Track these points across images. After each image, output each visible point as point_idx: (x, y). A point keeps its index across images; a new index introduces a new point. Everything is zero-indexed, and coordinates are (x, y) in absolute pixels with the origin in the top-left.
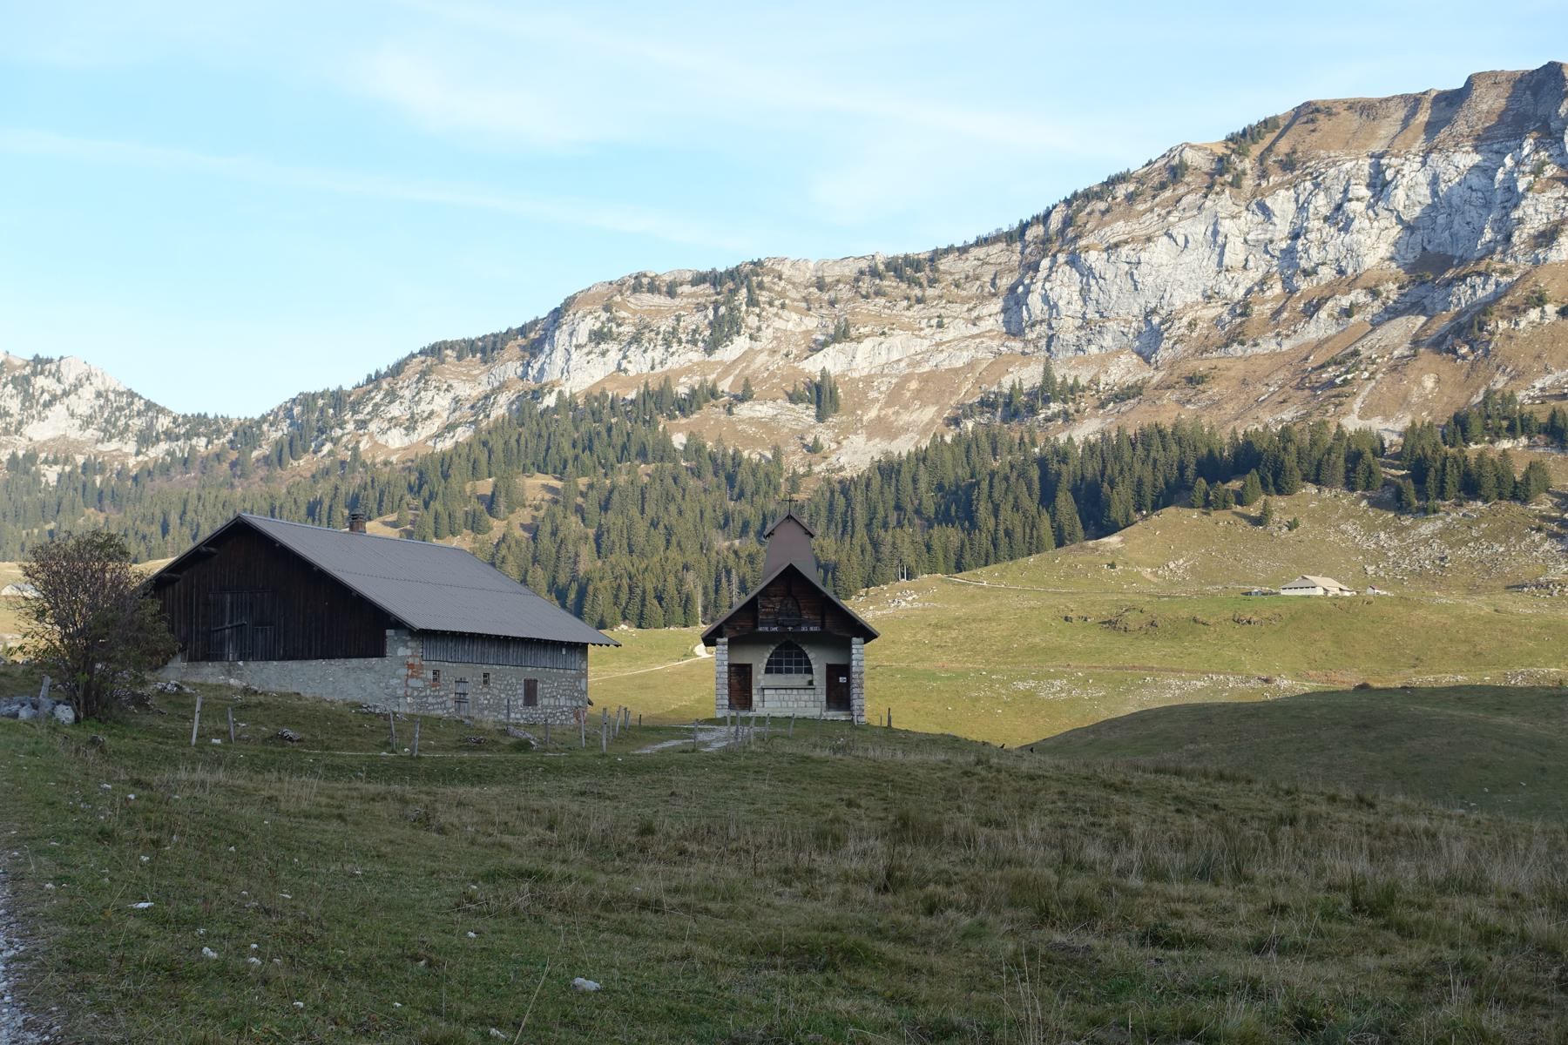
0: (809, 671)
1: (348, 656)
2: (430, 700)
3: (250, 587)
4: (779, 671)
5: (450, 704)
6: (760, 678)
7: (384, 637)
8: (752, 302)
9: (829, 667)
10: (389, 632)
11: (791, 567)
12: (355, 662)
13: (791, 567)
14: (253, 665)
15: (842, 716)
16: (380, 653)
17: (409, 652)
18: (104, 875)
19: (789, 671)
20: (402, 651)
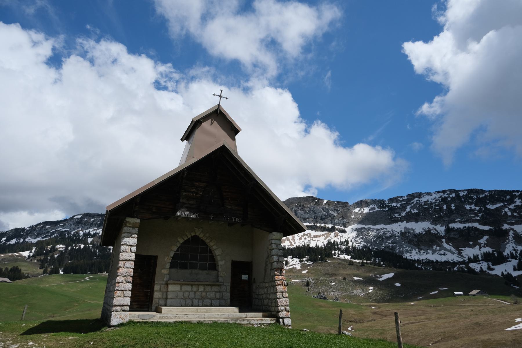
0: (214, 267)
4: (184, 266)
6: (163, 270)
9: (235, 264)
15: (255, 318)
19: (193, 267)
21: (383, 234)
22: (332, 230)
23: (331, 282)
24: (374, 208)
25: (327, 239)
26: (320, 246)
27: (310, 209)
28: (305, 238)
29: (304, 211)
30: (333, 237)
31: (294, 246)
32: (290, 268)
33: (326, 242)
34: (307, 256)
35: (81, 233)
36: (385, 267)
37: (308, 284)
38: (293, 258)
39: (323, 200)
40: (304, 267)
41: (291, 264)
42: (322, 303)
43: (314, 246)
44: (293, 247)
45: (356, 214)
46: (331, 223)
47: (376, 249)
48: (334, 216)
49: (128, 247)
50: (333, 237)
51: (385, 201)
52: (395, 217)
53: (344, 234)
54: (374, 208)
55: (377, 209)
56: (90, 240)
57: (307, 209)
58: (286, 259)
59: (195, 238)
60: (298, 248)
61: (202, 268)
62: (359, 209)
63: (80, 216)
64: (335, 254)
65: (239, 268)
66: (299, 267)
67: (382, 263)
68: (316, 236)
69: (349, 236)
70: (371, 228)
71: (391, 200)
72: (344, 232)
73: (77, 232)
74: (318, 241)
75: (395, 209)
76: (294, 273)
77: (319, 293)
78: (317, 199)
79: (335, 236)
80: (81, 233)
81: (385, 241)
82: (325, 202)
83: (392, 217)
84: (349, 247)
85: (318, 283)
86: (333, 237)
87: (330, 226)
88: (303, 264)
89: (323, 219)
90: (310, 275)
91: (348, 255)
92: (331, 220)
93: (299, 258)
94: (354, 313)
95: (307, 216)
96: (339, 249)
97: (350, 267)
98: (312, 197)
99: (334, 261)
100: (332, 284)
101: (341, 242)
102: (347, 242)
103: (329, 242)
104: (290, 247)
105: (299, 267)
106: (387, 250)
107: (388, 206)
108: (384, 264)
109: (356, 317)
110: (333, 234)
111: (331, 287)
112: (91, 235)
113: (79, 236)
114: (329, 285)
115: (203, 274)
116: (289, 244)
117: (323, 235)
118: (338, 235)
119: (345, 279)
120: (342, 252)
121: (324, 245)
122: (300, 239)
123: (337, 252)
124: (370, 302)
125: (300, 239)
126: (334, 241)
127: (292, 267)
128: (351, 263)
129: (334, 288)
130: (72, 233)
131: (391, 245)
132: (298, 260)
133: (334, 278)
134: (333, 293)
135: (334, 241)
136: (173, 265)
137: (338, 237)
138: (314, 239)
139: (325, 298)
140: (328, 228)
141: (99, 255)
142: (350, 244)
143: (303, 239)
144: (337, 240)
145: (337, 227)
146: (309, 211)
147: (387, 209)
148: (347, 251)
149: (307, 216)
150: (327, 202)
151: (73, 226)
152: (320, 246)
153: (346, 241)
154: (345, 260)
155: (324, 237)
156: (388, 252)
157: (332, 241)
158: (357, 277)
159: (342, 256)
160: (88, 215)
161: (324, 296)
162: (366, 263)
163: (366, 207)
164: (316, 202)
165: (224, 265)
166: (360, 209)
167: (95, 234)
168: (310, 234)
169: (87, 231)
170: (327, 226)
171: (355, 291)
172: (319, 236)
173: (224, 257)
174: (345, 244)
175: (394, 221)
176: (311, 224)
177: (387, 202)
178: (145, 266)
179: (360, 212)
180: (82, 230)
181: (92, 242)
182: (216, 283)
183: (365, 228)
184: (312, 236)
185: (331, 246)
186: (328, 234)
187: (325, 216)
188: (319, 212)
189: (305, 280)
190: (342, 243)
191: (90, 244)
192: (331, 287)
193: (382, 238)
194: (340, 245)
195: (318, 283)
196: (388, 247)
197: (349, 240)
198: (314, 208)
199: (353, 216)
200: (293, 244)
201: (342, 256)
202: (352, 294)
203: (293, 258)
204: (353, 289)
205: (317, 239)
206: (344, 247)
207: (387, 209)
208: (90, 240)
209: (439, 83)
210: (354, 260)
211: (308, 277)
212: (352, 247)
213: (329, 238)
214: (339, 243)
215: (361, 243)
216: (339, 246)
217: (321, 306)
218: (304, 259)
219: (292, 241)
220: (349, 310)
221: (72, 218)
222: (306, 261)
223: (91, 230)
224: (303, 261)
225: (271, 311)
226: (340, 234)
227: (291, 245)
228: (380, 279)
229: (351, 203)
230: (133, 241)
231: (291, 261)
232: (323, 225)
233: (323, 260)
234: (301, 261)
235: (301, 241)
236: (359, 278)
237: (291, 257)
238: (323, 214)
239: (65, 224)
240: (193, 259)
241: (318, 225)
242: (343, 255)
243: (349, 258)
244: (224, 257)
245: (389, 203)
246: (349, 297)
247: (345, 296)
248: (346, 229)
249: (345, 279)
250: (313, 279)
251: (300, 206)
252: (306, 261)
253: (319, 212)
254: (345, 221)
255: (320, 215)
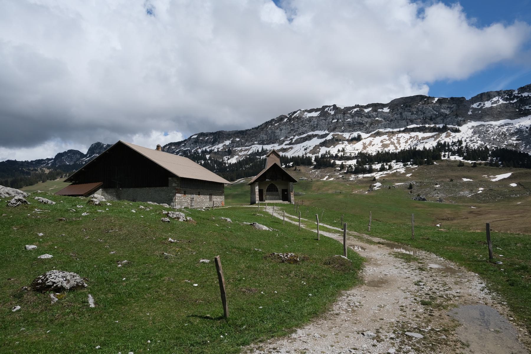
0: (277, 191)
1: (156, 186)
2: (183, 200)
3: (118, 168)
4: (270, 191)
5: (189, 201)
6: (265, 192)
7: (168, 180)
8: (219, 137)
9: (283, 190)
10: (170, 179)
11: (275, 164)
12: (158, 188)
13: (275, 164)
14: (125, 190)
15: (286, 202)
16: (167, 185)
17: (176, 185)
18: (39, 278)
19: (272, 191)
20: (174, 185)
21: (507, 130)
22: (444, 129)
23: (436, 184)
24: (498, 100)
25: (437, 140)
26: (428, 149)
27: (418, 109)
28: (412, 141)
29: (410, 112)
30: (444, 138)
31: (399, 150)
32: (393, 172)
33: (435, 144)
34: (412, 160)
35: (200, 151)
36: (503, 167)
37: (411, 187)
38: (396, 162)
39: (433, 98)
40: (408, 170)
41: (394, 168)
42: (420, 204)
43: (421, 149)
44: (397, 151)
45: (475, 110)
46: (443, 123)
47: (495, 148)
48: (446, 115)
49: (257, 189)
50: (443, 138)
51: (514, 91)
52: (526, 109)
53: (457, 134)
54: (498, 100)
55: (501, 102)
56: (208, 156)
57: (414, 110)
58: (389, 164)
59: (272, 184)
60: (403, 152)
61: (274, 191)
62: (478, 104)
63: (196, 136)
64: (444, 156)
65: (284, 191)
66: (402, 171)
67: (500, 163)
68: (423, 138)
69: (463, 135)
70: (491, 125)
71: (522, 90)
72: (458, 131)
73: (196, 150)
74: (426, 143)
75: (527, 99)
76: (396, 176)
77: (419, 195)
78: (426, 97)
79: (446, 137)
80: (200, 151)
81: (508, 138)
82: (436, 99)
83: (521, 110)
84: (462, 147)
85: (422, 185)
86: (444, 138)
87: (441, 126)
88: (407, 168)
89: (432, 119)
90: (414, 178)
91: (460, 156)
92: (443, 120)
93: (403, 162)
94: (449, 212)
95: (414, 117)
96: (449, 150)
97: (460, 168)
98: (421, 96)
99: (442, 163)
100: (437, 186)
101: (453, 142)
102: (460, 142)
103: (439, 144)
104: (395, 151)
105: (402, 171)
106: (510, 148)
107: (517, 97)
108: (502, 164)
109: (449, 216)
110: (444, 135)
111: (436, 190)
112: (208, 152)
113: (198, 153)
114: (433, 187)
115: (275, 193)
116: (394, 148)
117: (432, 137)
118: (450, 136)
119: (452, 180)
120: (454, 153)
121: (433, 147)
122: (406, 142)
123: (447, 153)
124: (478, 203)
125: (406, 142)
126: (445, 142)
127: (395, 171)
128: (461, 164)
129: (439, 190)
130: (193, 151)
131: (515, 142)
132: (402, 164)
133: (440, 180)
134: (437, 195)
135: (445, 142)
136: (267, 191)
137: (450, 137)
138: (421, 141)
139: (424, 200)
140: (439, 128)
141: (217, 169)
142: (464, 144)
143: (409, 142)
144: (449, 140)
145: (449, 126)
146: (417, 112)
147: (515, 101)
148: (459, 152)
149: (414, 117)
150: (438, 100)
151: (192, 145)
152: (428, 149)
153: (459, 141)
154: (455, 161)
155: (433, 139)
156: (511, 151)
157: (443, 142)
158: (467, 178)
159: (452, 158)
160: (202, 134)
161: (423, 198)
162: (480, 164)
163: (488, 100)
164: (425, 101)
165: (280, 190)
166: (480, 104)
167: (211, 151)
168: (417, 136)
169: (204, 149)
170: (437, 126)
171: (462, 193)
172: (428, 138)
173: (280, 188)
174: (458, 144)
175: (523, 114)
176: (418, 126)
177: (517, 92)
178: (261, 191)
179: (479, 107)
180: (200, 148)
181: (210, 158)
182: (278, 195)
183: (484, 125)
184: (420, 138)
185: (442, 147)
186: (439, 134)
187: (436, 115)
188: (429, 112)
189: (408, 184)
190: (454, 144)
191: (209, 160)
192: (436, 190)
193: (505, 135)
194: (452, 145)
195: (422, 185)
196: (511, 145)
197: (463, 140)
198: (423, 108)
199: (470, 113)
200: (398, 147)
201: (452, 158)
202: (458, 196)
203: (396, 162)
204: (460, 191)
205: (425, 141)
206: (456, 148)
207: (515, 101)
208: (208, 156)
209: (474, 27)
210: (466, 161)
211: (411, 180)
212: (466, 147)
213: (440, 139)
214: (450, 144)
215: (477, 143)
216: (450, 147)
217: (417, 207)
218: (409, 163)
219: (397, 145)
220: (446, 209)
221: (190, 138)
222: (411, 164)
223: (207, 147)
224: (407, 165)
225: (290, 201)
226: (453, 134)
227: (396, 149)
228: (494, 180)
229: (468, 98)
230: (257, 187)
231: (395, 165)
232: (432, 126)
233: (429, 163)
234: (404, 165)
235: (407, 144)
236: (469, 180)
237: (394, 161)
238: (433, 114)
239: (185, 144)
240: (272, 189)
241: (427, 126)
242: (454, 157)
243: (461, 159)
244: (280, 188)
245: (518, 94)
246: (454, 198)
247: (449, 197)
248: (460, 128)
249: (452, 180)
250: (416, 182)
251: (406, 107)
252: (411, 164)
253: (429, 112)
254: (460, 119)
255: (429, 115)
